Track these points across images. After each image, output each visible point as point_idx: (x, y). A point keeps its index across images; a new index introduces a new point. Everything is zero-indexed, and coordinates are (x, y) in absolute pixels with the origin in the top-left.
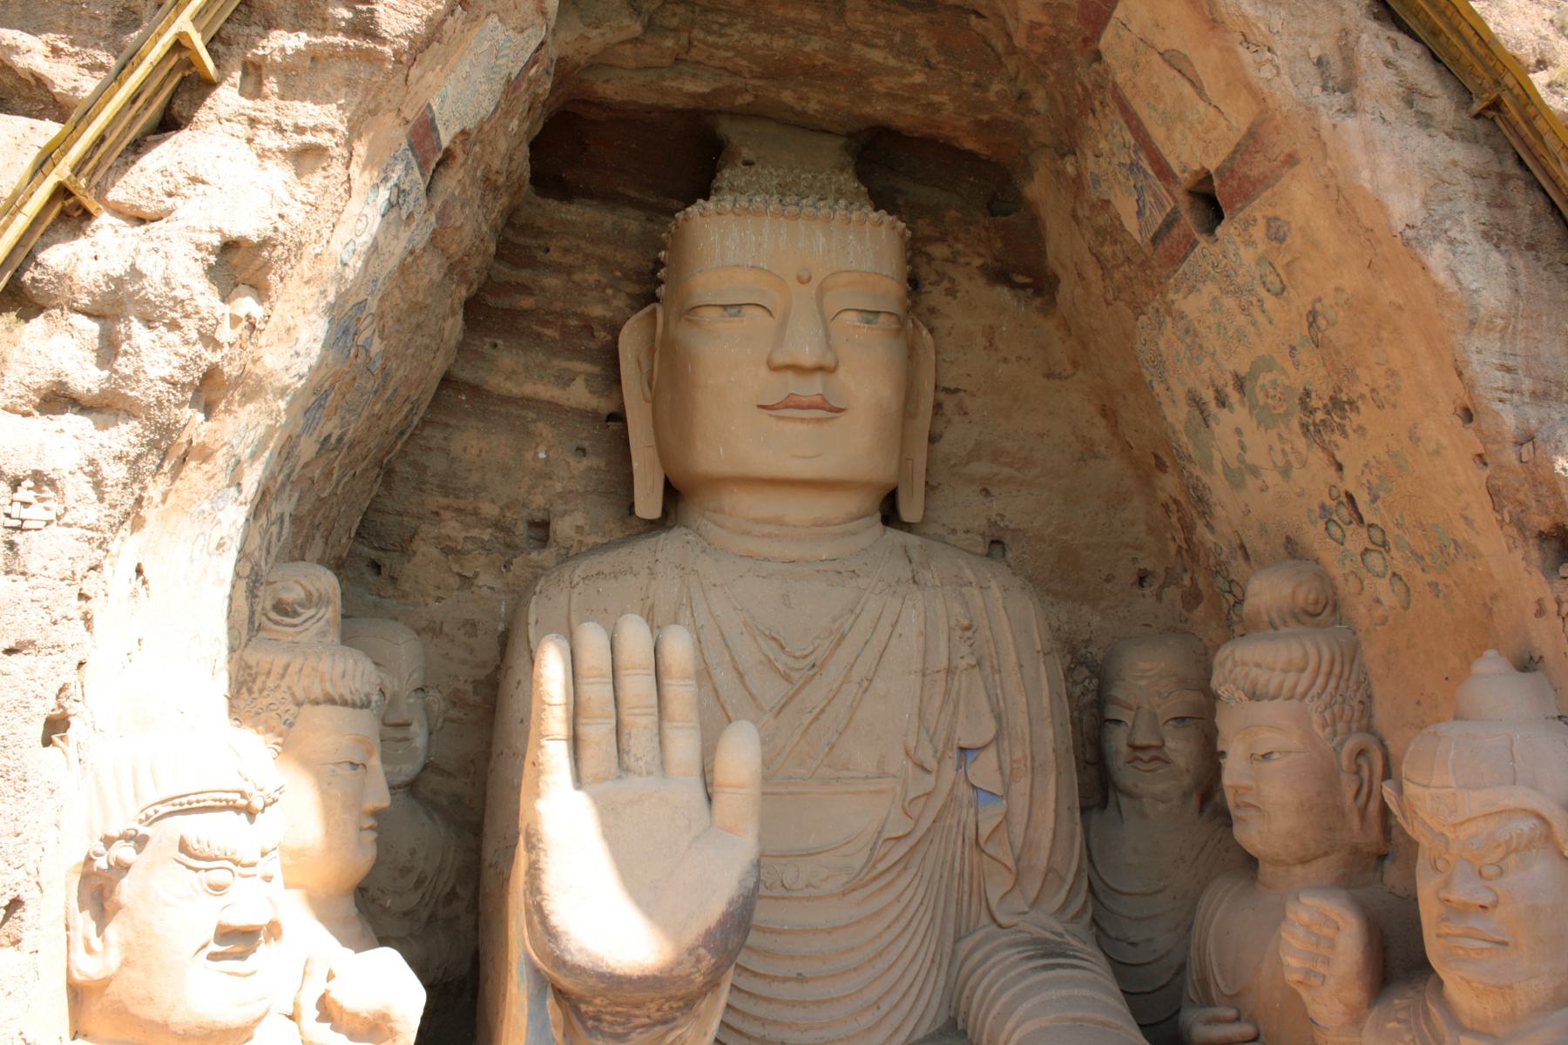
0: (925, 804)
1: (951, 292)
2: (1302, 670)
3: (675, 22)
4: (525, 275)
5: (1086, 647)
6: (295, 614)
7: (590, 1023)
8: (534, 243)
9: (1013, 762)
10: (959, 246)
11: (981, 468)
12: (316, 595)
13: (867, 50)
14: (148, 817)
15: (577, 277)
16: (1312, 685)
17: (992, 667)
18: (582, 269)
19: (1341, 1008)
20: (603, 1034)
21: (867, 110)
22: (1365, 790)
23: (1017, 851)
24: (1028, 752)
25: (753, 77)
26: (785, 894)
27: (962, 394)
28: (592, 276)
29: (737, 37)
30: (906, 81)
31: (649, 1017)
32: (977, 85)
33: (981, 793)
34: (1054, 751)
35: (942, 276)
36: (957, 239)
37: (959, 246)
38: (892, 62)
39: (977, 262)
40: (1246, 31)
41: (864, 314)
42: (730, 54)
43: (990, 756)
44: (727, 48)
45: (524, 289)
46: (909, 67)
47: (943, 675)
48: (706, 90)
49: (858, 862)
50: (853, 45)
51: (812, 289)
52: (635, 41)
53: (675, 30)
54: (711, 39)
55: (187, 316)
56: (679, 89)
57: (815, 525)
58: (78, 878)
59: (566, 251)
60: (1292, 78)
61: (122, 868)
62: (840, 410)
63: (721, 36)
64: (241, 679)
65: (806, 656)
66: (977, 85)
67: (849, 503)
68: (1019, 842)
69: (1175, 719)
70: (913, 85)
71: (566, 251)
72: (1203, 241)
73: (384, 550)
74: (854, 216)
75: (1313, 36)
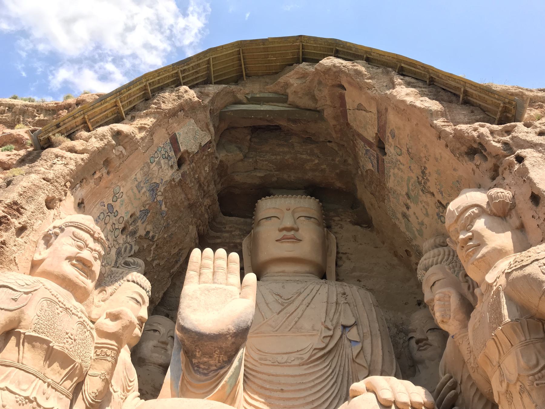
0: (330, 340)
1: (341, 227)
2: (439, 255)
3: (252, 156)
4: (219, 234)
5: (402, 326)
6: (129, 265)
7: (196, 368)
8: (222, 227)
9: (363, 333)
10: (343, 217)
11: (357, 274)
12: (136, 262)
13: (301, 155)
14: (66, 225)
15: (233, 233)
16: (443, 258)
17: (354, 305)
18: (235, 231)
19: (458, 323)
20: (200, 373)
21: (307, 177)
22: (471, 287)
23: (369, 363)
24: (369, 330)
25: (275, 171)
26: (278, 364)
27: (348, 254)
28: (237, 233)
29: (268, 157)
30: (314, 163)
31: (216, 366)
32: (333, 160)
33: (352, 342)
34: (379, 330)
35: (338, 224)
36: (342, 215)
37: (343, 217)
38: (308, 158)
39: (349, 220)
40: (368, 86)
41: (306, 218)
42: (267, 163)
43: (354, 330)
44: (266, 161)
45: (218, 237)
46: (313, 158)
47: (335, 304)
48: (263, 175)
49: (306, 357)
50: (298, 155)
51: (290, 211)
52: (242, 160)
53: (252, 157)
54: (261, 159)
55: (105, 139)
56: (256, 175)
57: (294, 273)
58: (43, 235)
59: (230, 227)
60: (380, 91)
61: (56, 235)
62: (301, 240)
63: (264, 158)
64: (109, 273)
65: (288, 299)
66: (333, 160)
67: (306, 268)
68: (369, 359)
69: (430, 329)
70: (315, 164)
71: (230, 227)
72: (384, 157)
73: (171, 310)
74: (303, 197)
75: (384, 82)
